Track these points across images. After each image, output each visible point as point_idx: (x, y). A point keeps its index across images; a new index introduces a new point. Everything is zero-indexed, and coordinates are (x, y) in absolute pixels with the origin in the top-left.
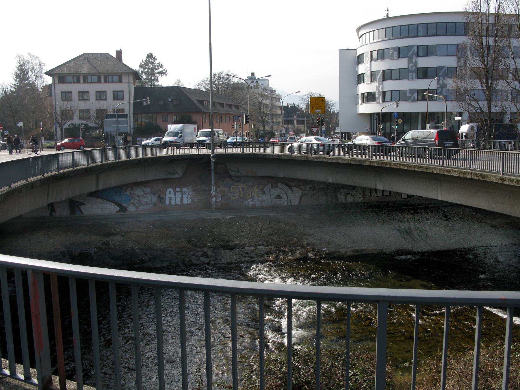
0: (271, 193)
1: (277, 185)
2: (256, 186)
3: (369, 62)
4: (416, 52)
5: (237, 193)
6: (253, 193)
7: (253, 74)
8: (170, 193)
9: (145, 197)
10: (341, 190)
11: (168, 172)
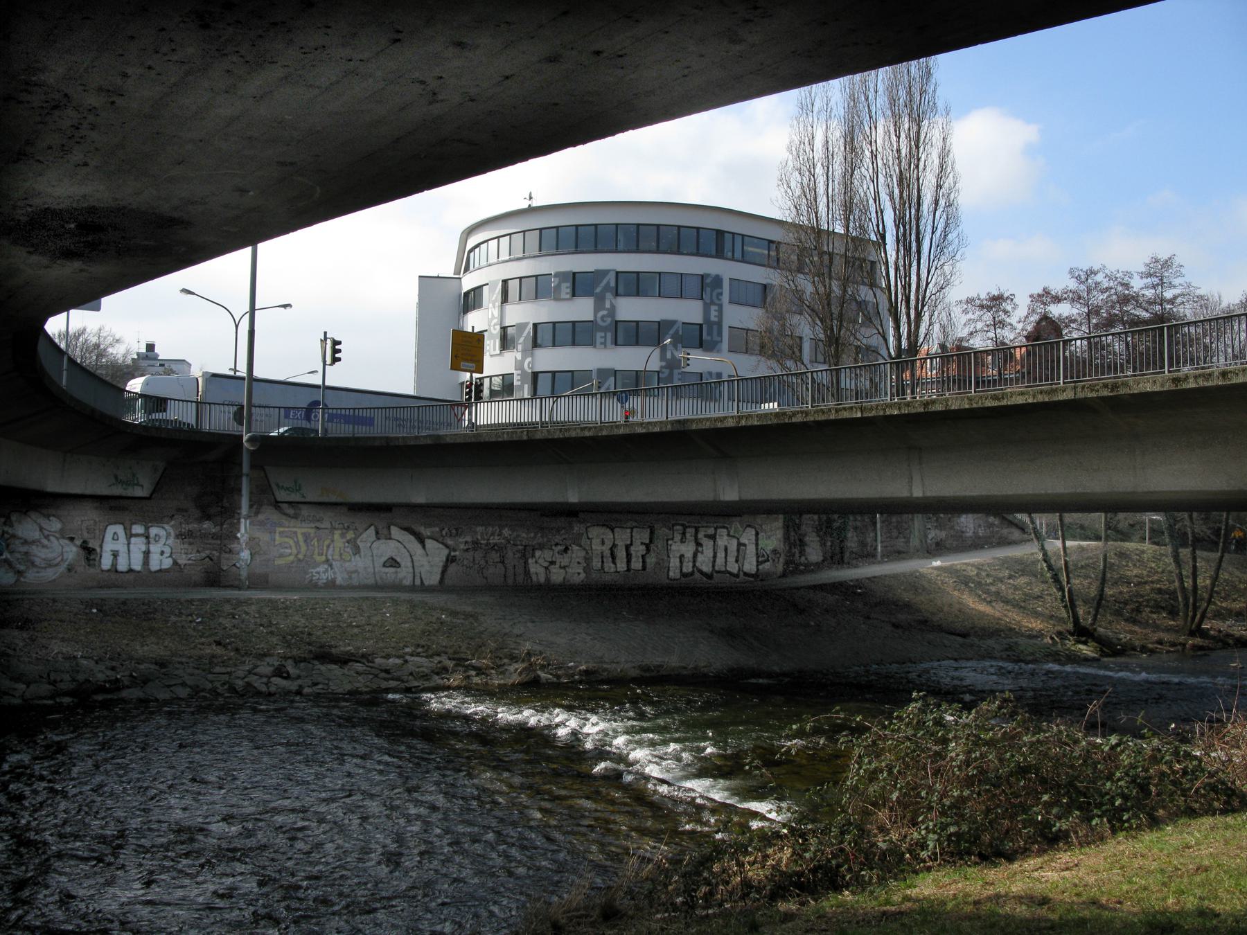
0: (375, 552)
1: (390, 534)
2: (340, 532)
3: (498, 304)
4: (613, 284)
5: (291, 547)
6: (331, 549)
7: (151, 347)
8: (115, 537)
9: (44, 546)
10: (538, 553)
11: (116, 477)
